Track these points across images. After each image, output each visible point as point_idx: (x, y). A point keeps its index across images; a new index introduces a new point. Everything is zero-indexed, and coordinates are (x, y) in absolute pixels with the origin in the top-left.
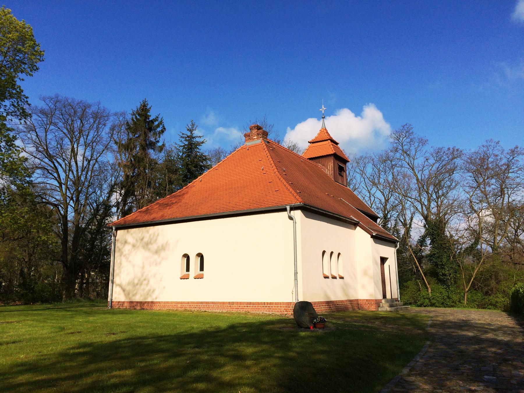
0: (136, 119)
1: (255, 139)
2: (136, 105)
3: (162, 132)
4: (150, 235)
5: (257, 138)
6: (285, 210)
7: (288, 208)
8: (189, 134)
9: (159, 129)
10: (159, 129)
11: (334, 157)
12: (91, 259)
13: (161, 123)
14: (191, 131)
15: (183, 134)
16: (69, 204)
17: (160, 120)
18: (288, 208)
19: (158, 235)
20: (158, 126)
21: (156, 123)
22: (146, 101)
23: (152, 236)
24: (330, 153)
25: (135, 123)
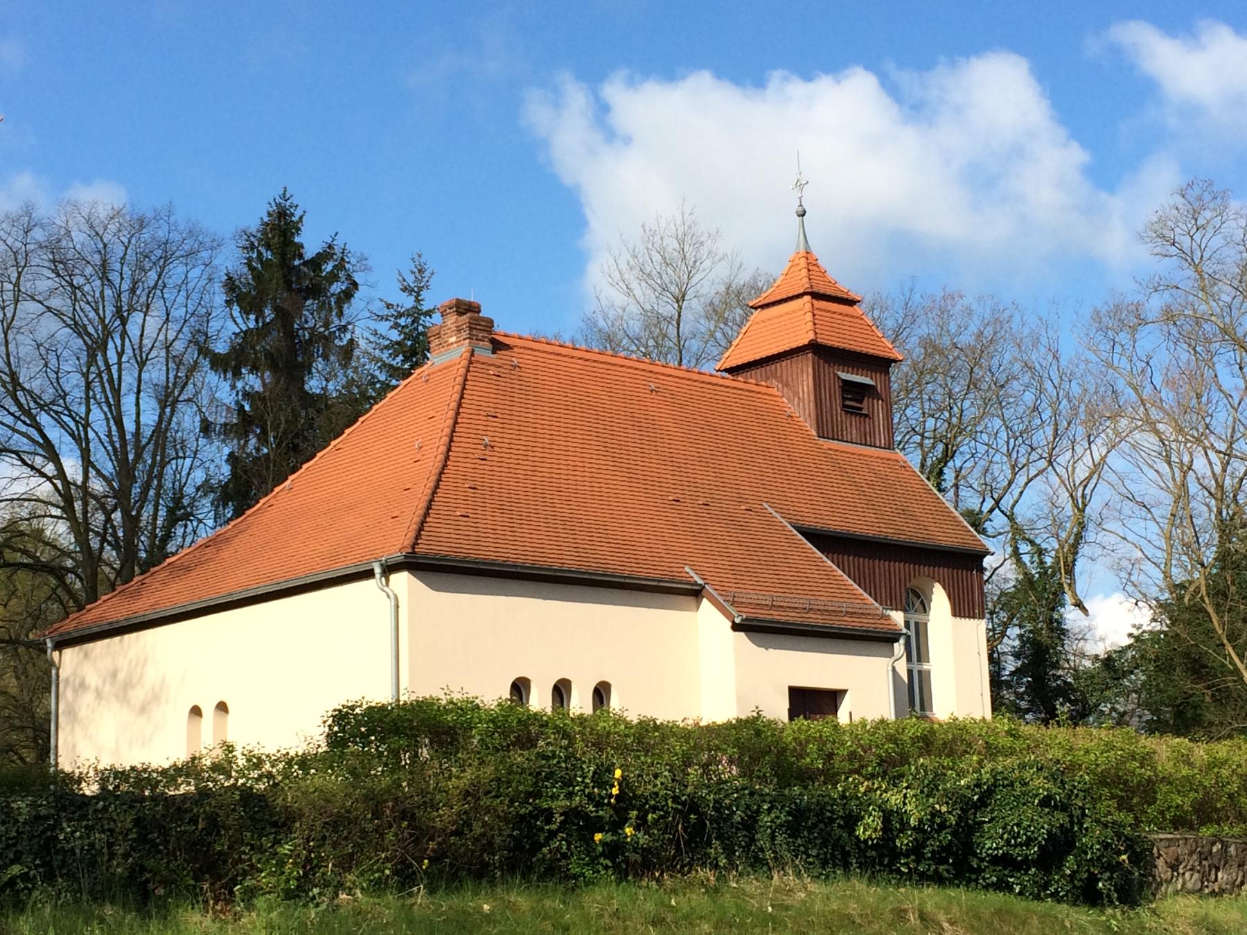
0: (262, 263)
1: (452, 344)
2: (254, 216)
3: (347, 295)
4: (130, 661)
5: (456, 342)
6: (369, 574)
7: (378, 570)
8: (408, 302)
9: (336, 288)
10: (336, 288)
11: (813, 353)
12: (723, 765)
13: (341, 265)
14: (415, 292)
15: (389, 306)
16: (100, 558)
17: (337, 250)
18: (378, 570)
19: (146, 660)
20: (333, 277)
21: (329, 267)
22: (288, 195)
23: (133, 664)
24: (800, 344)
25: (257, 276)
